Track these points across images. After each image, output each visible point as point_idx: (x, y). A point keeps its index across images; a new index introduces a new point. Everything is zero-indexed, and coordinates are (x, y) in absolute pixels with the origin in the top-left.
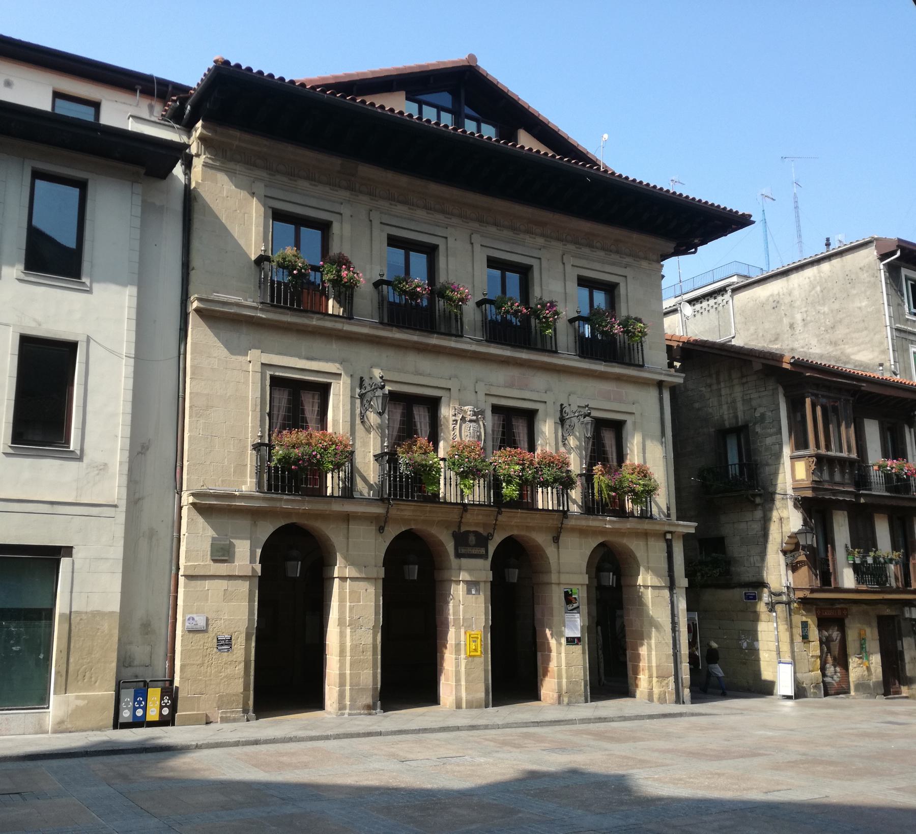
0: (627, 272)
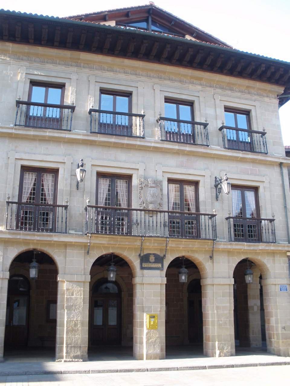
0: (257, 104)
